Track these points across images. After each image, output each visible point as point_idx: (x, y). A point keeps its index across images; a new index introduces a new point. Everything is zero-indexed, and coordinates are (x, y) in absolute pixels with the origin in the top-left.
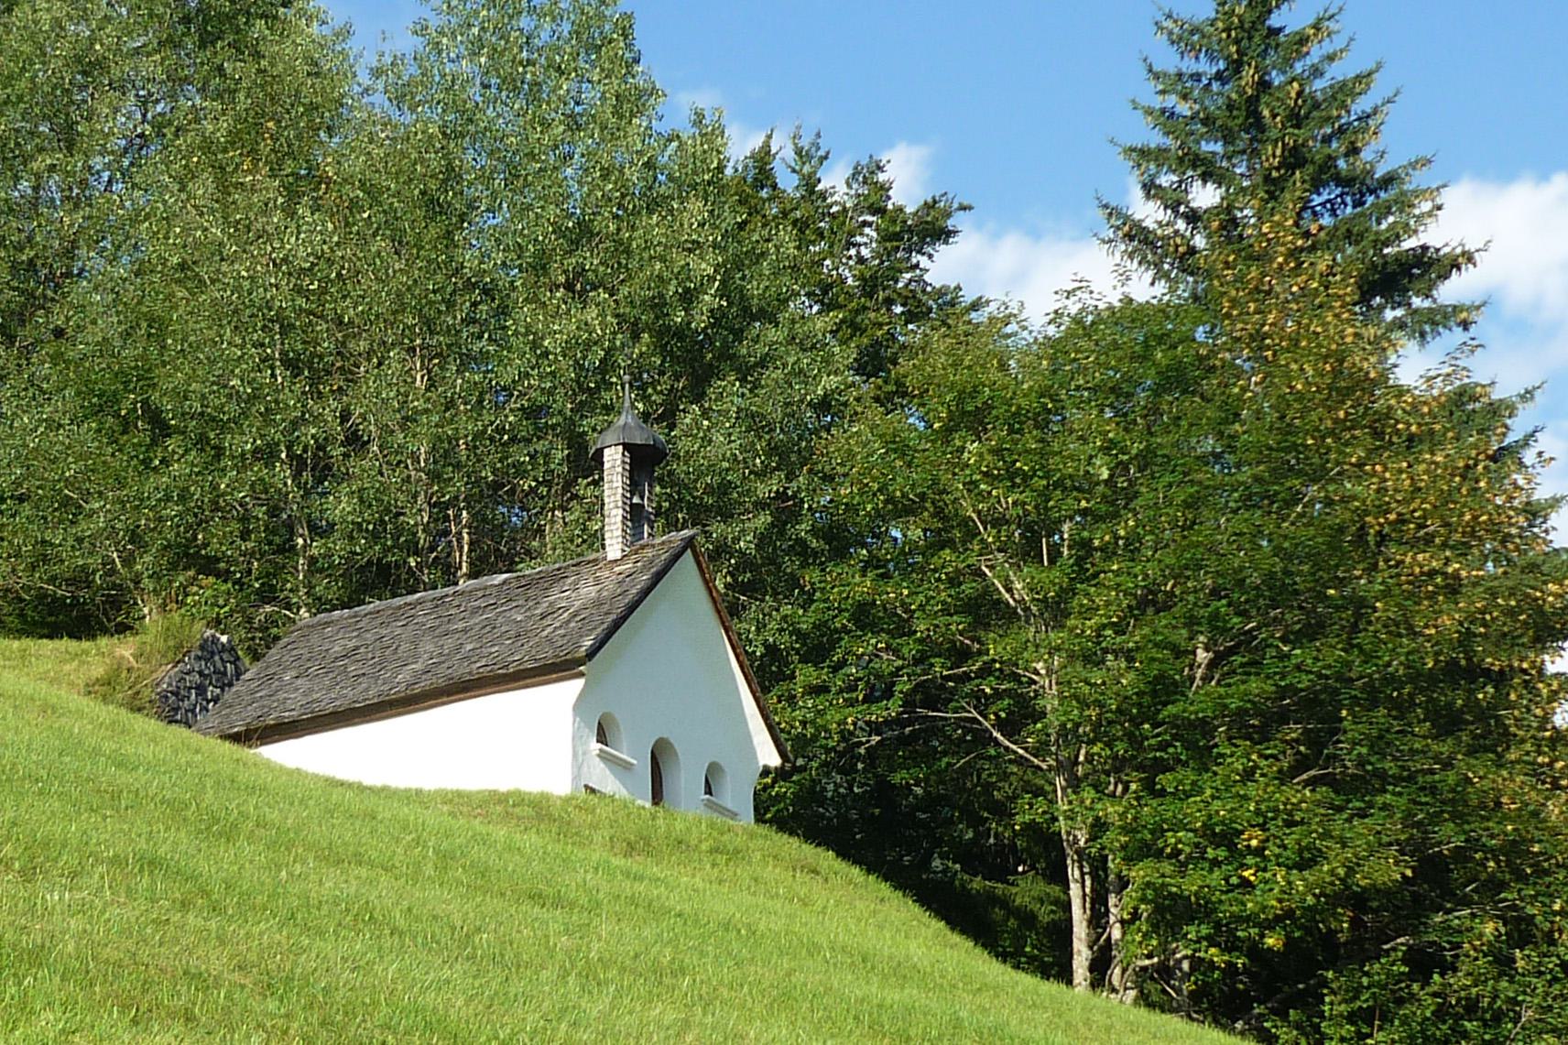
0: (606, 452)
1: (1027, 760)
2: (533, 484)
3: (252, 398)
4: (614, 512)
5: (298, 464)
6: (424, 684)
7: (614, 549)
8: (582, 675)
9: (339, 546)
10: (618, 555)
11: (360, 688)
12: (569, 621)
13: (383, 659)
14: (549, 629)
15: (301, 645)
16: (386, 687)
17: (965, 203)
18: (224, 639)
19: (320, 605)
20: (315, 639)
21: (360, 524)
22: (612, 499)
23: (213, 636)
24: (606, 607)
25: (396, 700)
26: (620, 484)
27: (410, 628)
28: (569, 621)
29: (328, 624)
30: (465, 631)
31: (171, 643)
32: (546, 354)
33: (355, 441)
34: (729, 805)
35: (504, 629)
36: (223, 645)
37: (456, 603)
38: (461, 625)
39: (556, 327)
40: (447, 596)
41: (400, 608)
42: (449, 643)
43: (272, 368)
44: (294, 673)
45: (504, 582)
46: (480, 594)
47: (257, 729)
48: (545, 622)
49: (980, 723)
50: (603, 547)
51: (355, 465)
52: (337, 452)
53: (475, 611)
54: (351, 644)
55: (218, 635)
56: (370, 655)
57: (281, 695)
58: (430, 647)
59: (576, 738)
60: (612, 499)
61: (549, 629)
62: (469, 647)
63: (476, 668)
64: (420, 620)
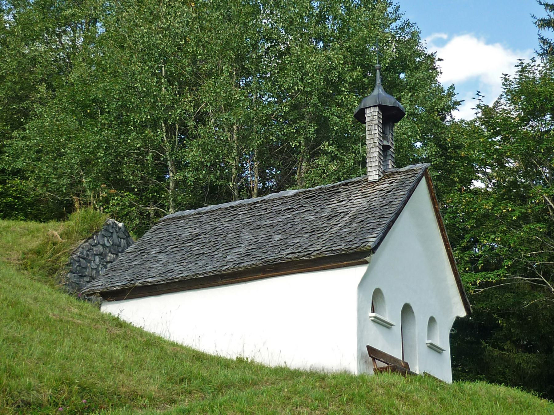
0: (367, 111)
1: (491, 288)
2: (298, 144)
3: (147, 94)
4: (373, 150)
5: (170, 130)
6: (248, 263)
7: (373, 175)
8: (366, 262)
9: (190, 175)
10: (377, 177)
11: (201, 263)
12: (351, 223)
13: (216, 244)
14: (336, 228)
15: (164, 231)
16: (218, 265)
17: (440, 58)
18: (121, 225)
19: (179, 206)
20: (172, 227)
21: (202, 162)
22: (372, 141)
23: (114, 223)
24: (378, 213)
25: (225, 275)
26: (377, 131)
27: (234, 222)
28: (351, 223)
29: (181, 218)
30: (272, 226)
31: (86, 226)
32: (306, 74)
33: (201, 119)
34: (387, 319)
35: (301, 226)
36: (120, 228)
37: (264, 207)
38: (268, 222)
39: (313, 59)
40: (257, 202)
41: (226, 209)
42: (262, 234)
43: (159, 79)
44: (157, 250)
45: (295, 195)
46: (280, 202)
47: (130, 289)
48: (333, 221)
49: (545, 283)
50: (365, 173)
51: (201, 131)
52: (191, 124)
53: (279, 212)
54: (195, 232)
55: (117, 222)
56: (208, 240)
57: (148, 265)
58: (249, 236)
59: (360, 310)
60: (372, 141)
61: (336, 228)
62: (277, 238)
63: (286, 254)
64: (241, 217)
